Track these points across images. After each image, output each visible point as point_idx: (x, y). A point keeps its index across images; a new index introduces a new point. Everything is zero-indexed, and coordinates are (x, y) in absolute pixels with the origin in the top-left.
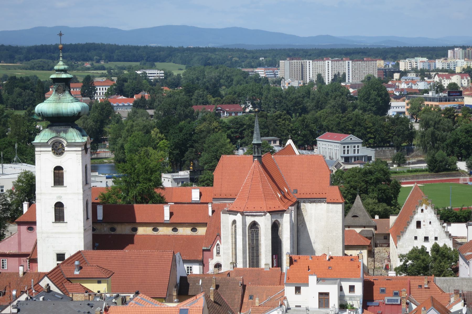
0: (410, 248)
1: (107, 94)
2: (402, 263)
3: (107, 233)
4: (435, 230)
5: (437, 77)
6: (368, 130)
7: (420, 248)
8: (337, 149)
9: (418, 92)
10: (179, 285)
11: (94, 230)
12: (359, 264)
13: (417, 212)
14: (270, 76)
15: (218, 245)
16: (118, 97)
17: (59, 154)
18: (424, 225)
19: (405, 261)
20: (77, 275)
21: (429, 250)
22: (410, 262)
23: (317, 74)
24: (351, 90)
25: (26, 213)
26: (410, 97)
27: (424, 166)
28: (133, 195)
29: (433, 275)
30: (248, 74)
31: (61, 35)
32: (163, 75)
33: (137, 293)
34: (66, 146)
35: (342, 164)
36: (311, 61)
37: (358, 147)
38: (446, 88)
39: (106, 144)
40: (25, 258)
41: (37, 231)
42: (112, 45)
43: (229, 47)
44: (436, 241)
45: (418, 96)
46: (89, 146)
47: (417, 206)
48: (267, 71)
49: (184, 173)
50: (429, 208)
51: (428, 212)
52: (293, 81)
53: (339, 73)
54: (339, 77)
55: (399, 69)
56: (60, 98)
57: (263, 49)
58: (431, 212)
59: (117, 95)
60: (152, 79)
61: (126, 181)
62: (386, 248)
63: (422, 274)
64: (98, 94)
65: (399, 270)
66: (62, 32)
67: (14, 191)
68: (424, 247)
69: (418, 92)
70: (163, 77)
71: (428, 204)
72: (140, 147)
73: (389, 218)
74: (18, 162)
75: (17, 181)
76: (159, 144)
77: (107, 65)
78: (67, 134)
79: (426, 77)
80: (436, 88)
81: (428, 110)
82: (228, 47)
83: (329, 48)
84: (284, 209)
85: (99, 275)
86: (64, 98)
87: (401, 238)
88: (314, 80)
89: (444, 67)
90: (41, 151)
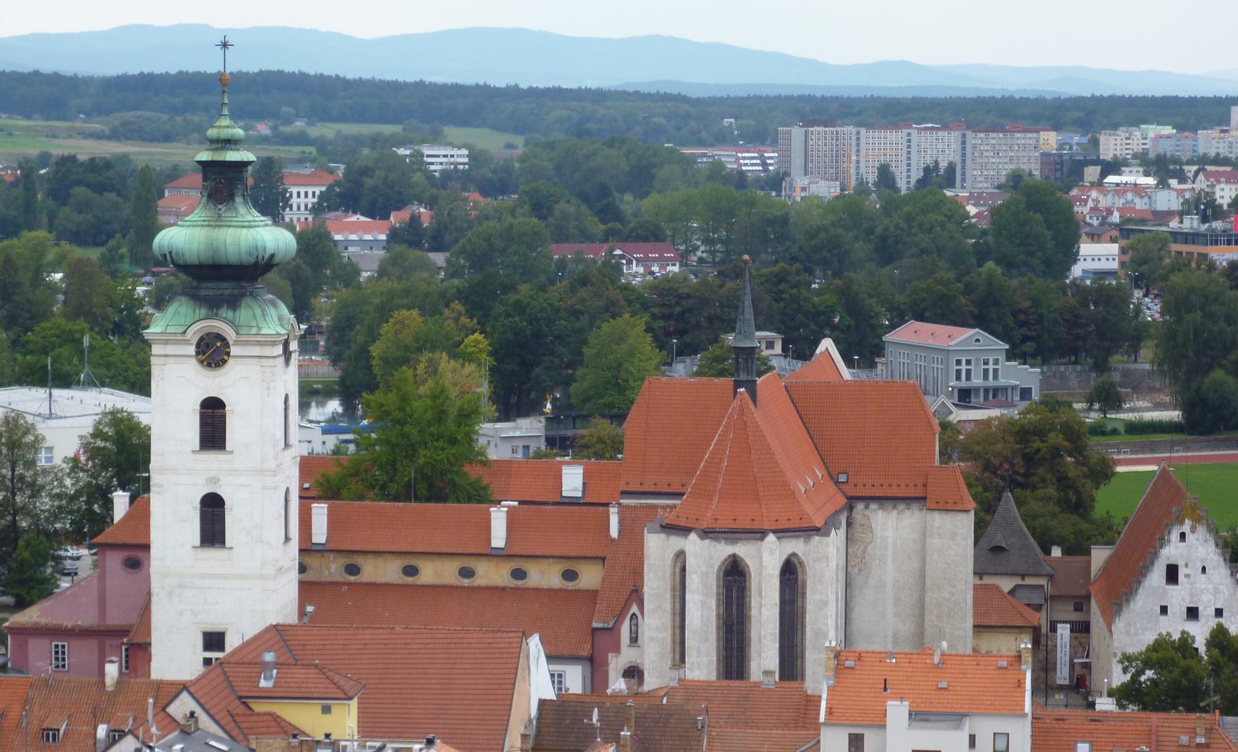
0: (1149, 638)
1: (317, 210)
2: (1128, 677)
3: (338, 578)
4: (1216, 591)
5: (1203, 179)
6: (1022, 317)
7: (1176, 636)
8: (906, 361)
9: (1150, 217)
10: (534, 722)
11: (302, 569)
12: (1020, 677)
13: (1169, 541)
14: (750, 168)
15: (634, 616)
16: (346, 217)
17: (216, 366)
18: (1187, 576)
19: (1137, 671)
20: (265, 690)
21: (1200, 644)
22: (1149, 674)
23: (877, 164)
24: (972, 210)
25: (119, 521)
26: (1132, 230)
27: (1175, 415)
28: (406, 479)
29: (1217, 712)
30: (695, 162)
31: (225, 45)
32: (466, 160)
33: (430, 742)
34: (233, 345)
35: (953, 408)
36: (863, 130)
37: (996, 362)
38: (1225, 207)
39: (317, 342)
40: (116, 642)
41: (152, 570)
42: (330, 77)
43: (642, 90)
44: (1220, 620)
45: (1154, 228)
46: (294, 346)
47: (1167, 525)
48: (746, 155)
49: (531, 423)
50: (1202, 530)
51: (1197, 540)
52: (814, 183)
53: (937, 163)
54: (937, 175)
55: (1098, 157)
56: (220, 216)
57: (731, 96)
58: (1206, 541)
59: (344, 211)
60: (436, 171)
61: (387, 442)
62: (1079, 635)
63: (1181, 708)
64: (295, 208)
65: (1125, 695)
66: (230, 40)
67: (83, 459)
68: (1188, 633)
69: (1150, 217)
70: (467, 166)
71: (1197, 520)
72: (412, 353)
73: (1089, 554)
74: (90, 384)
75: (91, 435)
76: (462, 346)
77: (315, 132)
78: (237, 313)
79: (1172, 177)
80: (1202, 207)
81: (1181, 263)
82: (637, 88)
83: (909, 95)
84: (1004, 545)
85: (326, 690)
86: (230, 215)
87: (1124, 609)
88: (871, 181)
89: (1221, 151)
90: (166, 356)
